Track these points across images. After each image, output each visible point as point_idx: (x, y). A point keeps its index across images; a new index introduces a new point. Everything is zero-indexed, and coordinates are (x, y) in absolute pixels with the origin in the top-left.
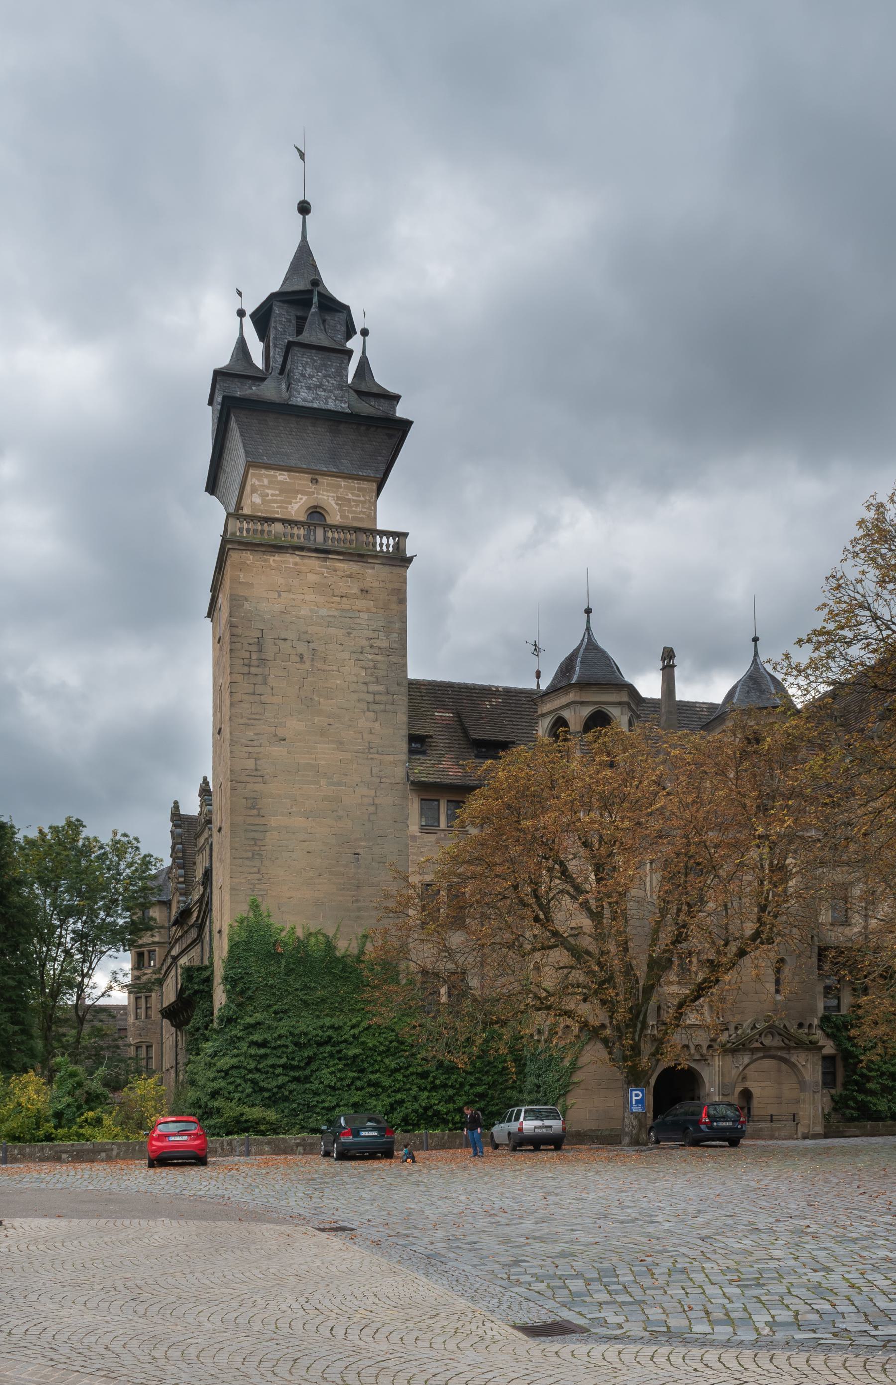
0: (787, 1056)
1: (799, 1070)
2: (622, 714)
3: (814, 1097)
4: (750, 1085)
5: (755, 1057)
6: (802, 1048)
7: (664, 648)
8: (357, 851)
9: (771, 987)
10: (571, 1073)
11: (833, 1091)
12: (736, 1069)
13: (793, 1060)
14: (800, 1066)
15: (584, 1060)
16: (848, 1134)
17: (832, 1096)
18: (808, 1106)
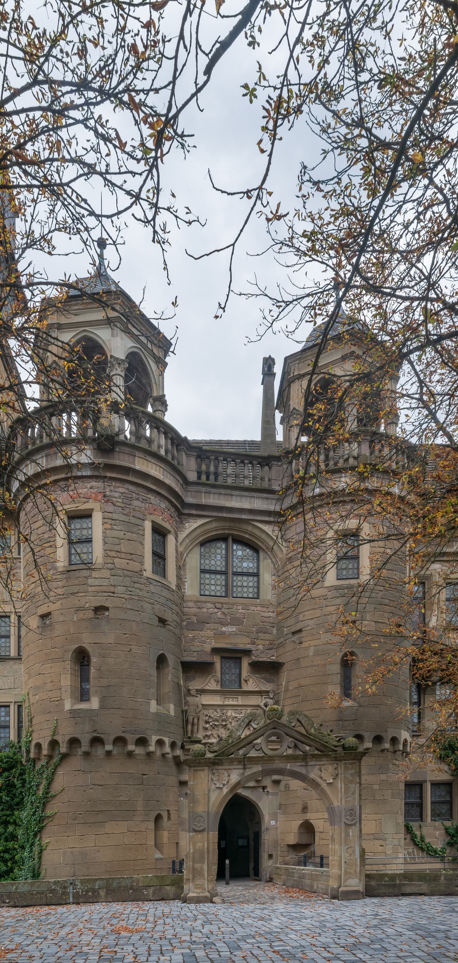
0: (303, 771)
1: (323, 792)
2: (113, 335)
3: (347, 834)
4: (311, 816)
5: (248, 772)
6: (326, 756)
7: (264, 358)
8: (362, 733)
9: (337, 690)
10: (44, 804)
11: (448, 824)
12: (217, 792)
13: (312, 776)
14: (324, 785)
15: (56, 786)
16: (408, 890)
17: (446, 829)
18: (337, 847)
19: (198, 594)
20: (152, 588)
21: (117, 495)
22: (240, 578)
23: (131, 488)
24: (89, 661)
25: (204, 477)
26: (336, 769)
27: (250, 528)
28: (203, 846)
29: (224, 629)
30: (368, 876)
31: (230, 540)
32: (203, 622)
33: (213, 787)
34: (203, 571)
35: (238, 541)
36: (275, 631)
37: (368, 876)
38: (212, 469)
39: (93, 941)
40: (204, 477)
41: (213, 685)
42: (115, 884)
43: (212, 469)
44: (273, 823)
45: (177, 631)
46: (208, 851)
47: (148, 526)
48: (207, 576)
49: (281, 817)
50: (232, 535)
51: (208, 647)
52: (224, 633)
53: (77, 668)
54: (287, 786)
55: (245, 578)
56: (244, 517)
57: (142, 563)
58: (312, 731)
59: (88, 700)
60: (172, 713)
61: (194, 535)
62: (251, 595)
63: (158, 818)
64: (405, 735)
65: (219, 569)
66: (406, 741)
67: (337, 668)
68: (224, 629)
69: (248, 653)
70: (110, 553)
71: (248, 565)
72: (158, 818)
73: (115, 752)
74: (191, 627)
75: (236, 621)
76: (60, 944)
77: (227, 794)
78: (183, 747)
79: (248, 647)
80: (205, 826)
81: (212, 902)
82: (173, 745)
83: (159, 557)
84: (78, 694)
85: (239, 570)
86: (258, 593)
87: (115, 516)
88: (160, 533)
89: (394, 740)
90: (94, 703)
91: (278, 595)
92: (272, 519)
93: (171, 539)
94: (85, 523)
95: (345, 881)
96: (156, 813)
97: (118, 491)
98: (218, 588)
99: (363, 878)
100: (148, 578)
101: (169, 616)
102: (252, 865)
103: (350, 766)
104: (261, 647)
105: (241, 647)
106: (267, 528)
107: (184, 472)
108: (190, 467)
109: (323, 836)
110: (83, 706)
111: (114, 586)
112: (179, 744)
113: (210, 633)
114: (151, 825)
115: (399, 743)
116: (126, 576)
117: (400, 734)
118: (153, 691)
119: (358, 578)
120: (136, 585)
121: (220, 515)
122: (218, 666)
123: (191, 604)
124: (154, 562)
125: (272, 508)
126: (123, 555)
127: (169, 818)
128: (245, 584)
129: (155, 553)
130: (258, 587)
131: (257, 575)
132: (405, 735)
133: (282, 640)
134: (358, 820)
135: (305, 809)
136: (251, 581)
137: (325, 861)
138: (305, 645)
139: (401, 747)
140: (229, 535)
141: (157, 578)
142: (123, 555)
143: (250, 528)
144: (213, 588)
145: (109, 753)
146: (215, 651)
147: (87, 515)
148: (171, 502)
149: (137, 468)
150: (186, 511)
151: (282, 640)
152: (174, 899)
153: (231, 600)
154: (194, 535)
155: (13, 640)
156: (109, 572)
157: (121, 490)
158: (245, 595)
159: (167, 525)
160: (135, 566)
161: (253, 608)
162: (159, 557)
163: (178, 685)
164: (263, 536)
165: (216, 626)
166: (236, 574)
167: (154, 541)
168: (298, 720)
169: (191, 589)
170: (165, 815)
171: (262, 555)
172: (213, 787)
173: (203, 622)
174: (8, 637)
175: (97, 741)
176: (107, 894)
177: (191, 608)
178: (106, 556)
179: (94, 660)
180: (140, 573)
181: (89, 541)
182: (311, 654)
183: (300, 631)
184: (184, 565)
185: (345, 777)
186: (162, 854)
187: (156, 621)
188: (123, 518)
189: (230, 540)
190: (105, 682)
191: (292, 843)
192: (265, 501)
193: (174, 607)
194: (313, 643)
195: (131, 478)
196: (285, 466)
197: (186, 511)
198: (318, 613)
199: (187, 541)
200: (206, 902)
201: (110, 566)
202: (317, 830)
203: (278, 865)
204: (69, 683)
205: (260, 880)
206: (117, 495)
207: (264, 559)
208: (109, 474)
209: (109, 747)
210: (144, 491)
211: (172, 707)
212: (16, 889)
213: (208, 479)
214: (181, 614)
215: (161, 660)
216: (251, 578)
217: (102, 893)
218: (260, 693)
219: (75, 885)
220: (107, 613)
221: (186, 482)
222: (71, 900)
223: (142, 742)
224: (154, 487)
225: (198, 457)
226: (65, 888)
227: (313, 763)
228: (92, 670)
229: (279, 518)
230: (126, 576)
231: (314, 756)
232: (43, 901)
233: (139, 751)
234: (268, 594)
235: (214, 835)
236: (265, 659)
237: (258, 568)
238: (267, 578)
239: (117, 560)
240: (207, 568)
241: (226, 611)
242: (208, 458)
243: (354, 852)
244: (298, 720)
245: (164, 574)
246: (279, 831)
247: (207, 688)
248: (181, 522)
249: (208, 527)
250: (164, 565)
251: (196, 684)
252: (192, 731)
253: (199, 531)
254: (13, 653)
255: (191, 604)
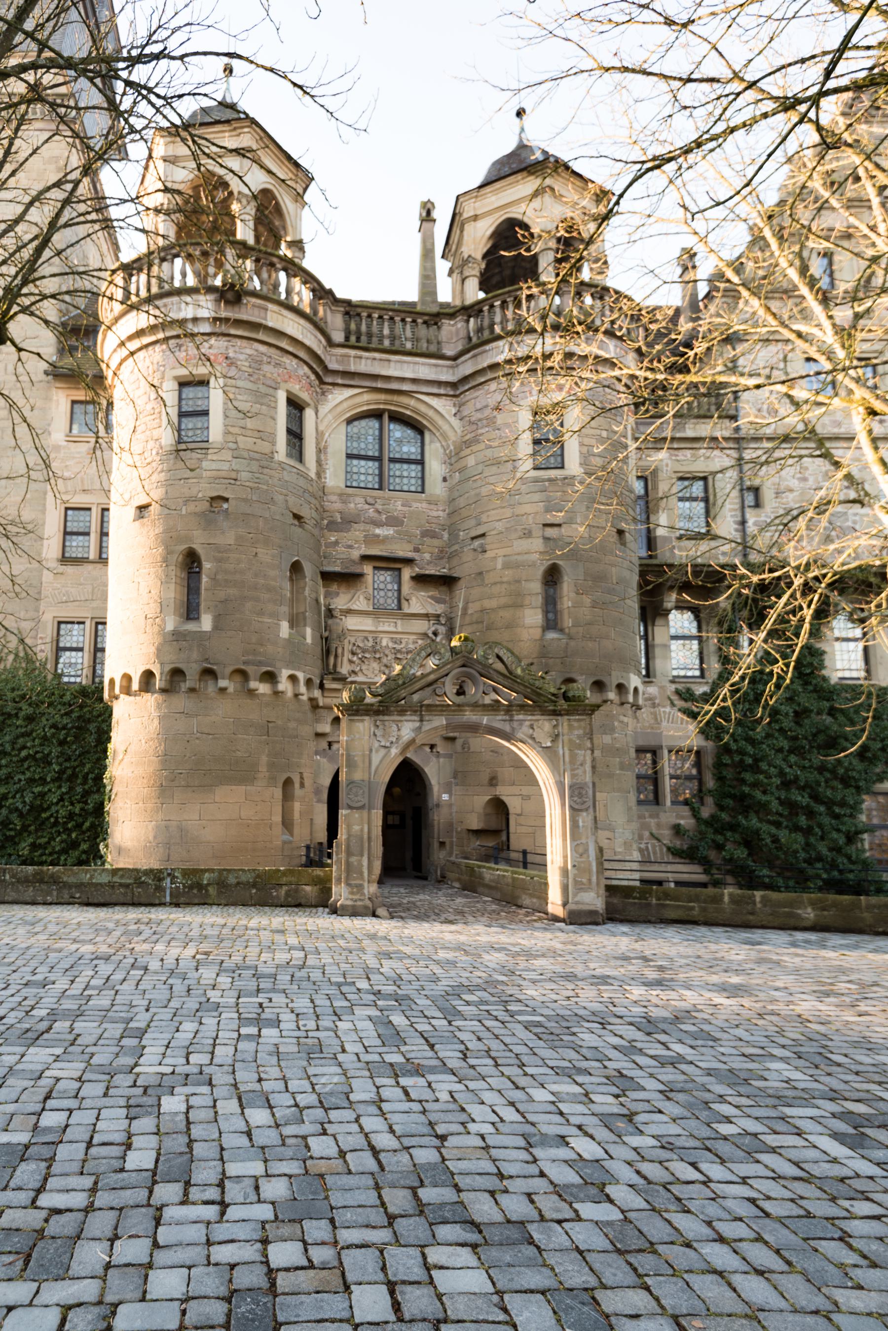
12: (383, 752)
19: (343, 486)
20: (286, 476)
21: (242, 357)
22: (398, 466)
23: (263, 348)
24: (200, 566)
25: (353, 338)
26: (555, 726)
27: (412, 402)
28: (362, 830)
29: (378, 531)
30: (609, 888)
31: (386, 417)
32: (349, 521)
33: (376, 744)
34: (350, 456)
35: (396, 418)
36: (446, 536)
37: (609, 888)
38: (364, 328)
39: (219, 979)
40: (353, 338)
41: (360, 604)
42: (232, 880)
43: (364, 328)
44: (445, 797)
45: (316, 532)
46: (369, 838)
47: (282, 397)
48: (355, 462)
49: (457, 790)
50: (389, 411)
51: (356, 554)
52: (378, 536)
53: (184, 575)
54: (465, 745)
55: (405, 466)
56: (405, 387)
57: (274, 443)
58: (519, 671)
59: (197, 619)
60: (309, 640)
61: (340, 409)
62: (413, 489)
63: (288, 783)
64: (634, 681)
65: (370, 453)
66: (636, 689)
67: (536, 586)
68: (378, 531)
69: (409, 561)
70: (231, 430)
71: (410, 450)
72: (288, 783)
73: (231, 690)
74: (332, 526)
75: (394, 521)
76: (170, 981)
77: (396, 756)
78: (321, 686)
79: (410, 555)
80: (365, 801)
81: (374, 915)
82: (309, 682)
83: (295, 435)
84: (184, 610)
85: (397, 456)
86: (423, 485)
87: (240, 383)
88: (295, 406)
89: (621, 688)
90: (206, 623)
91: (451, 490)
92: (442, 391)
93: (309, 413)
94: (199, 391)
95: (575, 895)
96: (284, 776)
97: (243, 351)
98: (370, 478)
99: (602, 891)
100: (280, 463)
101: (306, 512)
102: (409, 855)
103: (576, 724)
104: (427, 556)
105: (401, 554)
106: (434, 402)
107: (328, 330)
108: (336, 323)
109: (522, 820)
110: (191, 626)
111: (237, 471)
112: (317, 681)
113: (360, 535)
114: (278, 793)
115: (627, 692)
116: (252, 459)
117: (628, 680)
118: (284, 609)
119: (562, 467)
120: (266, 471)
121: (374, 385)
122: (369, 579)
123: (334, 498)
124: (289, 443)
125: (444, 378)
126: (249, 433)
127: (302, 785)
128: (405, 474)
129: (289, 431)
130: (423, 478)
131: (421, 462)
132: (634, 681)
133: (456, 547)
134: (591, 803)
135: (493, 781)
136: (414, 470)
137: (530, 858)
138: (489, 554)
139: (631, 699)
140: (384, 410)
141: (292, 462)
142: (249, 433)
143: (412, 402)
144: (362, 478)
145: (223, 690)
146: (365, 558)
147: (203, 383)
148: (311, 368)
149: (270, 324)
150: (329, 379)
151: (456, 547)
152: (316, 906)
153: (387, 494)
154: (340, 409)
155: (94, 537)
156: (230, 453)
157: (249, 351)
158: (405, 488)
159: (305, 396)
160: (265, 447)
161: (415, 505)
162: (295, 435)
163: (317, 601)
164: (431, 413)
165: (368, 527)
166: (392, 460)
167: (289, 415)
168: (498, 657)
169: (334, 479)
170: (296, 780)
171: (427, 436)
172: (376, 744)
173: (349, 521)
174: (87, 534)
175: (209, 673)
176: (220, 893)
177: (334, 505)
178: (227, 433)
179: (207, 565)
180: (270, 456)
181: (205, 413)
182: (499, 566)
183: (483, 535)
184: (325, 448)
185: (570, 740)
186: (292, 835)
187: (290, 520)
188: (250, 385)
189: (386, 417)
190: (221, 594)
191: (475, 827)
192: (434, 369)
193: (313, 500)
194: (501, 552)
195: (261, 336)
196: (459, 325)
197: (329, 379)
198: (508, 513)
199: (330, 417)
200: (366, 915)
201: (233, 446)
202: (512, 811)
203: (453, 859)
204: (172, 595)
205: (425, 878)
206: (242, 357)
207: (431, 442)
208: (233, 331)
209: (222, 683)
210: (278, 352)
211: (309, 631)
212: (92, 877)
213: (358, 339)
214: (322, 510)
215: (296, 568)
216: (413, 467)
217: (212, 890)
218: (427, 616)
219: (174, 877)
220: (225, 506)
221: (331, 343)
222: (168, 899)
223: (270, 677)
224: (291, 349)
225: (347, 313)
226: (160, 880)
227: (521, 717)
228: (204, 579)
229: (455, 389)
230: (252, 459)
231: (523, 707)
232: (128, 899)
233: (263, 688)
234: (436, 487)
235: (377, 815)
236: (432, 572)
237: (422, 453)
238: (435, 467)
239: (240, 439)
240: (355, 452)
241: (380, 507)
242: (359, 315)
243: (586, 851)
244: (498, 657)
245: (300, 458)
246: (454, 809)
247: (355, 607)
248: (323, 393)
249: (358, 400)
250: (301, 447)
251: (340, 602)
252: (335, 665)
253: (345, 405)
254: (93, 555)
255: (334, 498)
